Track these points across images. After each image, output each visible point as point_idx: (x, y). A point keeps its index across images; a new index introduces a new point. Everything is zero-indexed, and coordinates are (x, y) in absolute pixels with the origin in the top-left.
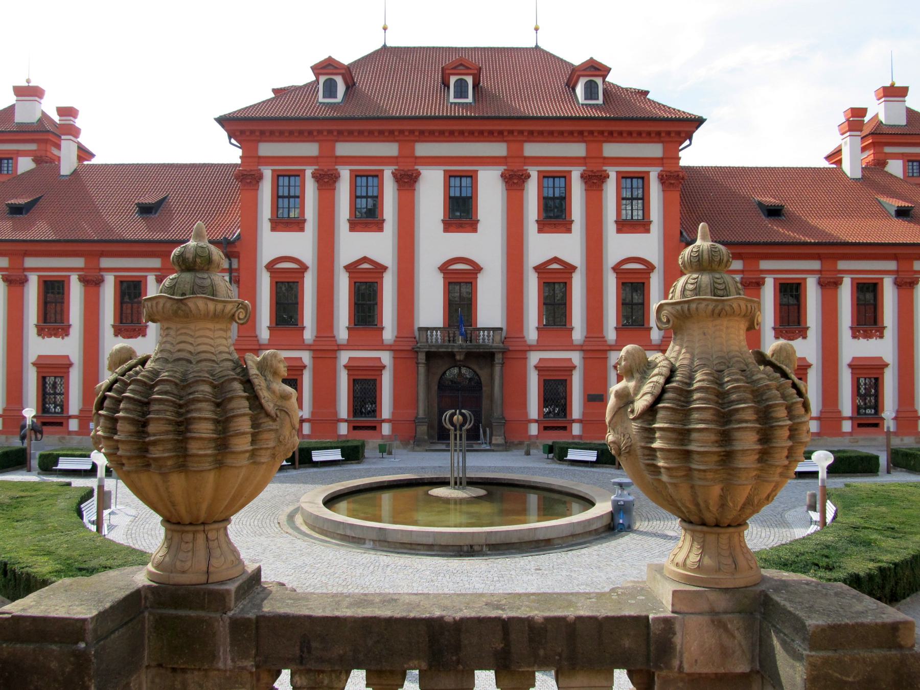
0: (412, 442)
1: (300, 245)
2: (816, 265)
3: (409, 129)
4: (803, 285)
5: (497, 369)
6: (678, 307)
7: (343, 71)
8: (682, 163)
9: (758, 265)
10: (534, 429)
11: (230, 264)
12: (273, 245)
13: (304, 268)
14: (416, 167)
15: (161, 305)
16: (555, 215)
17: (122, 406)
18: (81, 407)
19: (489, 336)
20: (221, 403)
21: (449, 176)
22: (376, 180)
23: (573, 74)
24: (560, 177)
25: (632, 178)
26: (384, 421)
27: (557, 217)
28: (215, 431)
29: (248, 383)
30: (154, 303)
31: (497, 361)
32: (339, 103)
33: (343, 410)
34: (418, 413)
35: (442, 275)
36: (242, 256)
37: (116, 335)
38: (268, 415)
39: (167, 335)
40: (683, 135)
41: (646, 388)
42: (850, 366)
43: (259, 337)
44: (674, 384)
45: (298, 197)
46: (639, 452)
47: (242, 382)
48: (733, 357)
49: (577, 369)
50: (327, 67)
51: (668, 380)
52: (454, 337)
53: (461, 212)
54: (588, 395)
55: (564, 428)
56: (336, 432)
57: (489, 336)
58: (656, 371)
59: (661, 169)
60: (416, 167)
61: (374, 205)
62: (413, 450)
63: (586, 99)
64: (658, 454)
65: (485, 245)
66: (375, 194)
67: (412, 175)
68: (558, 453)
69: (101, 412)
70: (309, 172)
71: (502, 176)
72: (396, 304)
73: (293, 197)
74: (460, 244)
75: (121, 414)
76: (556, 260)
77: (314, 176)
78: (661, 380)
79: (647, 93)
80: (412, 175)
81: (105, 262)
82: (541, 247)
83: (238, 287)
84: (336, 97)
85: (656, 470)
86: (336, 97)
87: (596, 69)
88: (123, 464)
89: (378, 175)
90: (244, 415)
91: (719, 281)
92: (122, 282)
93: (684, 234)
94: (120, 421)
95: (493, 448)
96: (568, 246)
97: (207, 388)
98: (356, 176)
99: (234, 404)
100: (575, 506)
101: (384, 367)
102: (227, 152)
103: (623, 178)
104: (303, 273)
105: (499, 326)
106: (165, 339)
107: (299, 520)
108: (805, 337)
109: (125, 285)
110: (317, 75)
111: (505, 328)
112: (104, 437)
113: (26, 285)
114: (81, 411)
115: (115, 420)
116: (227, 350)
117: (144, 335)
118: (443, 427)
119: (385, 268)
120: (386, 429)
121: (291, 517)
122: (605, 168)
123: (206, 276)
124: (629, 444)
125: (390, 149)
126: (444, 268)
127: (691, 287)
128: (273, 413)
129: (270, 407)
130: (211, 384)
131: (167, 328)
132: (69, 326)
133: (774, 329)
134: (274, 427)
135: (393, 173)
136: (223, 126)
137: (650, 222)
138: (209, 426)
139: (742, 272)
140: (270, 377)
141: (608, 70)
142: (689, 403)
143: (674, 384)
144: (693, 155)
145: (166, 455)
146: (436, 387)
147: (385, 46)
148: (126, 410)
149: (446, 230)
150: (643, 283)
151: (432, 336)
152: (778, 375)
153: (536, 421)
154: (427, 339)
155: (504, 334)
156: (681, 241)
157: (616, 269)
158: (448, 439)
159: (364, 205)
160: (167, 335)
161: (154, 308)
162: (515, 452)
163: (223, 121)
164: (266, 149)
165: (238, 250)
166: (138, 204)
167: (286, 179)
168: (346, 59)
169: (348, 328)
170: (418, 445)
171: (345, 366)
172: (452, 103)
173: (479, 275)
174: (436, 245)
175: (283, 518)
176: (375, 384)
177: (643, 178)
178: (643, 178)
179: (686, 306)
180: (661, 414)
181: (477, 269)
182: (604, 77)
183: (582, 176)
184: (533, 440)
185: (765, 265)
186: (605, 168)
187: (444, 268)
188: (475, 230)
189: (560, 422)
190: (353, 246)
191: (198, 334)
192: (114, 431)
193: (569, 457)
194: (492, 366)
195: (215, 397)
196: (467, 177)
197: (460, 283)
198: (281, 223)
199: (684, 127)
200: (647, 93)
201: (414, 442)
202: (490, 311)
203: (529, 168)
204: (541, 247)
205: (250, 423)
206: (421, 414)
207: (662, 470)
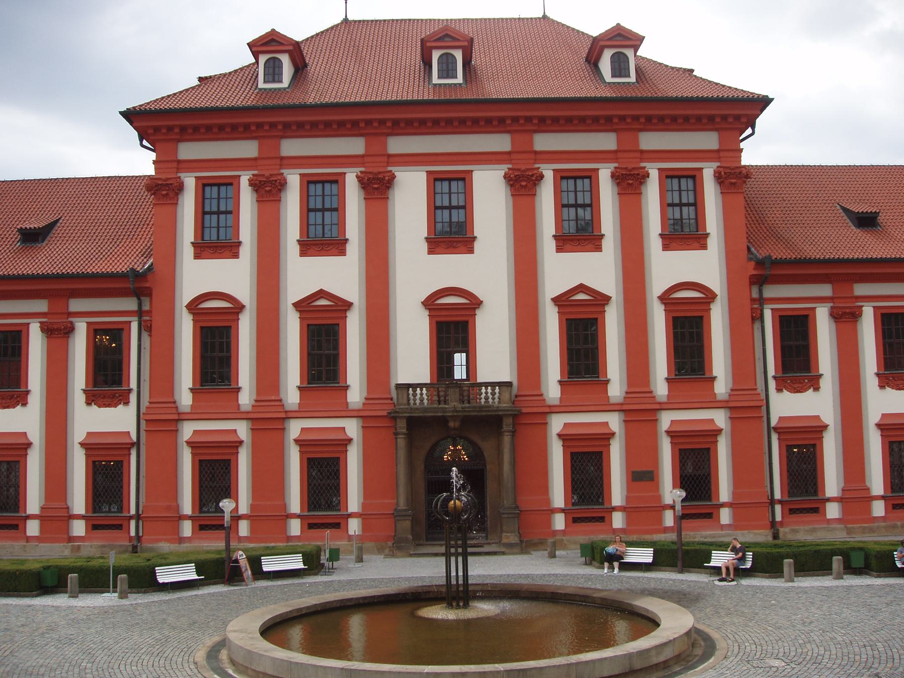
0: (390, 543)
1: (234, 277)
2: (825, 290)
3: (375, 120)
4: (810, 318)
5: (507, 439)
7: (291, 48)
9: (852, 290)
10: (559, 522)
11: (140, 305)
12: (197, 277)
13: (239, 308)
14: (389, 168)
18: (842, 485)
19: (493, 394)
21: (434, 179)
22: (335, 187)
24: (583, 178)
25: (679, 177)
26: (723, 505)
31: (505, 428)
32: (285, 89)
33: (295, 502)
34: (397, 504)
35: (427, 313)
36: (154, 293)
40: (744, 120)
42: (878, 425)
43: (178, 404)
45: (669, 205)
49: (831, 428)
50: (268, 44)
52: (445, 396)
53: (451, 233)
56: (178, 533)
57: (493, 394)
59: (718, 164)
60: (389, 168)
62: (393, 556)
63: (612, 76)
65: (485, 272)
67: (383, 179)
68: (596, 555)
70: (244, 181)
71: (505, 177)
74: (451, 270)
76: (582, 288)
77: (252, 183)
80: (383, 179)
81: (76, 305)
82: (561, 271)
83: (150, 336)
84: (281, 81)
86: (281, 81)
89: (591, 176)
93: (753, 249)
95: (503, 549)
96: (599, 270)
98: (308, 182)
100: (621, 626)
101: (350, 440)
103: (667, 177)
104: (238, 313)
105: (507, 379)
107: (224, 655)
110: (256, 55)
111: (515, 383)
113: (71, 335)
114: (42, 508)
117: (25, 404)
119: (349, 305)
120: (354, 526)
121: (213, 654)
122: (643, 165)
126: (430, 303)
132: (28, 392)
133: (878, 375)
135: (357, 177)
136: (131, 123)
137: (707, 235)
141: (641, 39)
144: (759, 150)
146: (422, 467)
149: (431, 252)
151: (415, 395)
153: (562, 510)
154: (409, 400)
156: (750, 260)
157: (665, 298)
162: (535, 554)
164: (188, 151)
165: (144, 285)
166: (21, 230)
167: (215, 189)
168: (298, 34)
170: (399, 548)
171: (297, 441)
172: (435, 85)
174: (419, 273)
175: (200, 655)
176: (338, 463)
177: (204, 185)
178: (695, 176)
181: (475, 303)
182: (636, 48)
183: (613, 176)
184: (558, 537)
185: (861, 289)
186: (643, 165)
187: (430, 303)
188: (471, 251)
190: (304, 275)
194: (499, 434)
196: (457, 179)
198: (206, 248)
199: (739, 111)
201: (398, 546)
202: (493, 358)
203: (542, 166)
204: (561, 271)
206: (402, 505)
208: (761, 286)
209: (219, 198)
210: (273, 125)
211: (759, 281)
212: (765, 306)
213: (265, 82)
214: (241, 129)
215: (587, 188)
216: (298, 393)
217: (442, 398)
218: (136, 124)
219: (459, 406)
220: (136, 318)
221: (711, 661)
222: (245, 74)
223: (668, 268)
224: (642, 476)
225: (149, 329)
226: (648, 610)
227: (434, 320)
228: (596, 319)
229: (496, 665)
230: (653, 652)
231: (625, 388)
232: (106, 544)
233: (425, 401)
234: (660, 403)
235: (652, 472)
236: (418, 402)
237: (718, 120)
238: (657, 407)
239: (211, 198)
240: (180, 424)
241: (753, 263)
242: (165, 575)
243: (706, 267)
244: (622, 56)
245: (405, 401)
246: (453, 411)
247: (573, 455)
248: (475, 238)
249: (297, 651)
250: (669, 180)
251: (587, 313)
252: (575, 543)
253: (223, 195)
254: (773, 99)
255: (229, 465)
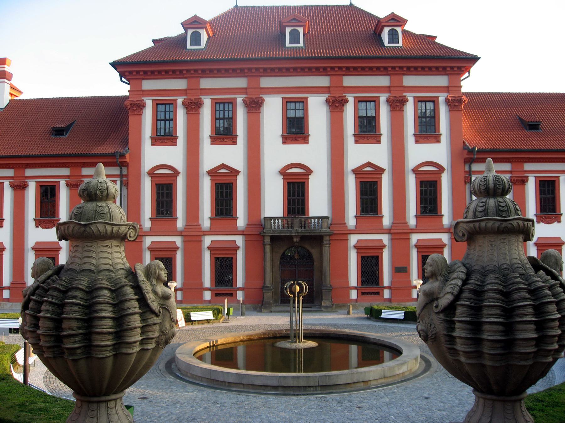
1: (173, 156)
4: (438, 182)
6: (471, 225)
8: (464, 90)
9: (523, 167)
10: (354, 294)
11: (121, 171)
12: (153, 156)
15: (71, 229)
16: (367, 130)
17: (43, 307)
20: (119, 305)
21: (287, 102)
22: (230, 106)
23: (379, 24)
24: (371, 101)
27: (370, 132)
28: (115, 327)
29: (138, 289)
30: (66, 226)
31: (325, 242)
32: (202, 49)
33: (207, 281)
34: (264, 283)
35: (282, 177)
37: (37, 226)
38: (152, 312)
39: (76, 251)
41: (448, 288)
44: (469, 286)
45: (172, 120)
46: (443, 339)
47: (133, 287)
48: (515, 263)
49: (387, 247)
51: (465, 282)
53: (295, 130)
54: (396, 268)
55: (378, 293)
56: (202, 298)
58: (455, 275)
61: (230, 124)
63: (389, 43)
64: (458, 340)
65: (314, 154)
66: (230, 116)
67: (258, 101)
68: (374, 314)
69: (27, 312)
72: (246, 199)
73: (167, 120)
74: (296, 153)
75: (43, 314)
76: (223, 166)
78: (460, 283)
79: (435, 37)
80: (258, 101)
81: (29, 172)
82: (358, 154)
83: (127, 189)
84: (200, 45)
85: (454, 352)
86: (200, 45)
87: (395, 20)
88: (44, 352)
90: (135, 314)
91: (502, 204)
92: (41, 186)
94: (41, 319)
96: (378, 154)
97: (107, 293)
98: (215, 103)
99: (128, 304)
102: (118, 88)
103: (419, 101)
106: (74, 254)
108: (559, 222)
109: (44, 188)
111: (330, 216)
112: (30, 331)
114: (11, 283)
115: (37, 319)
116: (121, 261)
118: (284, 293)
119: (383, 170)
122: (404, 94)
123: (103, 204)
124: (434, 332)
125: (240, 83)
126: (283, 172)
127: (481, 209)
128: (157, 310)
129: (155, 305)
130: (110, 289)
131: (76, 246)
134: (158, 321)
136: (116, 69)
138: (109, 322)
139: (510, 172)
140: (154, 282)
142: (482, 301)
143: (469, 286)
144: (473, 83)
145: (76, 346)
147: (236, 6)
148: (46, 310)
149: (284, 142)
150: (436, 181)
152: (549, 277)
153: (355, 288)
154: (271, 226)
155: (330, 222)
156: (465, 149)
157: (415, 171)
158: (289, 303)
159: (222, 125)
160: (76, 251)
161: (66, 231)
163: (115, 65)
164: (148, 85)
167: (163, 106)
168: (208, 15)
169: (210, 218)
171: (208, 248)
173: (310, 177)
174: (278, 154)
176: (232, 260)
179: (477, 224)
180: (459, 310)
181: (308, 171)
183: (388, 101)
185: (528, 167)
187: (283, 172)
188: (306, 142)
189: (374, 288)
190: (213, 156)
191: (102, 255)
192: (37, 326)
193: (383, 316)
195: (113, 299)
196: (300, 102)
197: (296, 188)
199: (463, 62)
200: (435, 37)
202: (318, 205)
204: (358, 154)
205: (140, 319)
207: (461, 353)
208: (471, 164)
209: (165, 112)
210: (196, 71)
211: (470, 161)
212: (473, 176)
213: (290, 43)
214: (178, 73)
215: (373, 107)
216: (209, 221)
217: (290, 225)
218: (119, 70)
219: (300, 230)
220: (119, 179)
221: (427, 373)
222: (180, 41)
223: (418, 154)
224: (400, 270)
225: (127, 185)
226: (397, 346)
227: (359, 180)
228: (377, 182)
229: (315, 373)
230: (396, 368)
231: (392, 221)
232: (82, 303)
233: (280, 227)
234: (411, 229)
235: (406, 268)
236: (276, 227)
237: (329, 69)
238: (410, 231)
239: (161, 112)
240: (203, 238)
241: (466, 151)
242: (385, 314)
243: (438, 152)
244: (394, 31)
245: (269, 227)
246: (296, 233)
247: (362, 257)
248: (177, 137)
249: (208, 363)
250: (420, 103)
251: (372, 178)
252: (362, 306)
253: (168, 110)
254: (480, 58)
255: (172, 261)
